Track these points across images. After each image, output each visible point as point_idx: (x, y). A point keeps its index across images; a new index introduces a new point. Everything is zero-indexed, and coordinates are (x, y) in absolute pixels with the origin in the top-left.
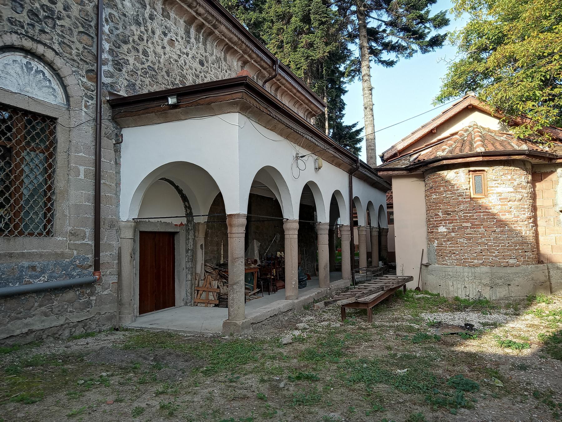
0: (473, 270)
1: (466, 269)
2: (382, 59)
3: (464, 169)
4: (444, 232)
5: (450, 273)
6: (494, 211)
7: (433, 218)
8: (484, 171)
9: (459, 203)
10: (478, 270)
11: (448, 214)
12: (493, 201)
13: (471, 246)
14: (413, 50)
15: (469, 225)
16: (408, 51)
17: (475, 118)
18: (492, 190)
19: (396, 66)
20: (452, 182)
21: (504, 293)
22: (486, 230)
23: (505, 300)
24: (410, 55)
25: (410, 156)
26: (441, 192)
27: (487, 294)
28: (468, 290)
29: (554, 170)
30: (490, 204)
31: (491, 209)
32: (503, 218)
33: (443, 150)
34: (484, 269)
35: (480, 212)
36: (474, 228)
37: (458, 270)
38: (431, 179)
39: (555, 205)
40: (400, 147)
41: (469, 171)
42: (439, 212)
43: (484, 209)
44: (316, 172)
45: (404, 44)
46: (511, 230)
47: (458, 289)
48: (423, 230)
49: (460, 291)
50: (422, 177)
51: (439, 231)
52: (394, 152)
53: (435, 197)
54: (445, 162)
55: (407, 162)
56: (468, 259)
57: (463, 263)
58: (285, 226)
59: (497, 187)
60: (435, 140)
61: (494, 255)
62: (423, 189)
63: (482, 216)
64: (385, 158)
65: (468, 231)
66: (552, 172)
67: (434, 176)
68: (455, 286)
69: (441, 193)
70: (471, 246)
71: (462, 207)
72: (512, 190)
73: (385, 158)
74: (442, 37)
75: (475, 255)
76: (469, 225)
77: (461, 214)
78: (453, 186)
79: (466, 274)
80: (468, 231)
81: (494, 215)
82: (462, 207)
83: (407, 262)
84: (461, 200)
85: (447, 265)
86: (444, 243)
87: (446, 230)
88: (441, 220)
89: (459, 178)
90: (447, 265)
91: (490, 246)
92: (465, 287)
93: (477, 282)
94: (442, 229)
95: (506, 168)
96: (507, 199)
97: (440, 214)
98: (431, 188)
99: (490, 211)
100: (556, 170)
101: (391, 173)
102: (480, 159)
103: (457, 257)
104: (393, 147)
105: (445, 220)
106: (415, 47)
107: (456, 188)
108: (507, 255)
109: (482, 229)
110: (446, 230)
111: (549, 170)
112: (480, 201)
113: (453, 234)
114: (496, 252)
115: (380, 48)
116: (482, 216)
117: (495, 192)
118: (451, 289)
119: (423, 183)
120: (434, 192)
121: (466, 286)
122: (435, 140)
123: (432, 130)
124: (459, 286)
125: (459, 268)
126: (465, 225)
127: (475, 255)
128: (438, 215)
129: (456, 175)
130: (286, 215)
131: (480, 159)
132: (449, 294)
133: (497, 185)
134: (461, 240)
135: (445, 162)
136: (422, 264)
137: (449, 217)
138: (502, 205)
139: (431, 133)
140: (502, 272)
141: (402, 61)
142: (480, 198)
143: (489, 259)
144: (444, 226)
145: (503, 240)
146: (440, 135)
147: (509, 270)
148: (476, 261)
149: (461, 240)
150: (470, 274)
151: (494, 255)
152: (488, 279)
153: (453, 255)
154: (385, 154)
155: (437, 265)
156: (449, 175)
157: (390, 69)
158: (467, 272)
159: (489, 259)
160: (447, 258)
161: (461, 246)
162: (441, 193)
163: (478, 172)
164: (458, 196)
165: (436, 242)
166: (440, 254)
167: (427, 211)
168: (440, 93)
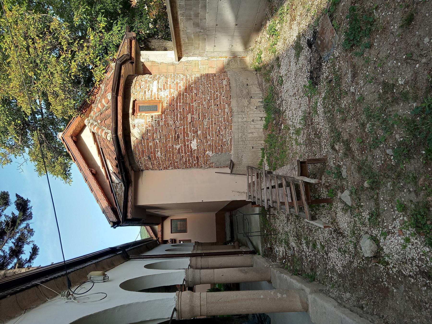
0: (235, 114)
1: (235, 119)
2: (28, 259)
3: (130, 119)
4: (197, 142)
5: (240, 136)
6: (175, 94)
7: (183, 157)
8: (134, 102)
9: (167, 124)
10: (234, 109)
11: (178, 137)
12: (166, 95)
13: (212, 115)
14: (26, 228)
15: (189, 116)
16: (26, 232)
17: (87, 137)
18: (155, 95)
19: (38, 246)
20: (144, 131)
21: (255, 88)
22: (195, 101)
23: (262, 86)
24: (31, 232)
25: (112, 182)
26: (154, 144)
27: (257, 101)
28: (256, 118)
29: (142, 64)
30: (169, 97)
31: (174, 97)
32: (183, 88)
33: (106, 133)
34: (234, 103)
35: (177, 106)
36: (193, 111)
37: (236, 127)
38: (141, 159)
39: (173, 64)
40: (105, 203)
41: (133, 114)
42: (176, 149)
43: (173, 105)
44: (108, 281)
45: (18, 235)
46: (195, 83)
47: (255, 128)
48: (195, 172)
49: (257, 126)
50: (138, 172)
51: (196, 148)
52: (110, 210)
53: (159, 153)
54: (120, 132)
55: (119, 186)
56: (224, 117)
57: (229, 123)
58: (186, 316)
59: (152, 91)
60: (103, 171)
61: (219, 95)
62: (150, 172)
63: (181, 104)
64: (115, 220)
65: (196, 116)
66: (144, 65)
67: (136, 154)
68: (253, 131)
69: (155, 146)
70: (212, 115)
71: (171, 123)
72: (156, 82)
73: (115, 220)
74: (18, 200)
75: (220, 111)
76: (189, 116)
77: (178, 123)
78: (147, 131)
79: (240, 120)
80: (196, 116)
81: (179, 94)
82: (171, 123)
83: (229, 188)
84: (163, 123)
85: (231, 139)
86: (209, 143)
87: (195, 140)
88: (185, 145)
89: (139, 125)
90: (231, 139)
91: (211, 97)
92: (253, 121)
93: (246, 110)
94: (194, 145)
95: (133, 84)
96: (164, 85)
97: (178, 147)
98: (150, 158)
99: (175, 97)
100: (142, 62)
101: (129, 204)
102: (120, 98)
103: (222, 128)
104: (104, 212)
105: (184, 141)
106: (23, 225)
107: (150, 128)
108: (219, 85)
109: (194, 104)
110: (195, 140)
111: (142, 67)
112: (165, 105)
113: (199, 132)
114: (216, 93)
115: (15, 260)
116: (181, 104)
117: (156, 93)
118: (255, 135)
119: (145, 173)
120: (155, 154)
121: (252, 119)
122: (103, 171)
123: (93, 174)
124: (252, 126)
125: (234, 126)
126: (189, 120)
127: (220, 111)
128: (179, 149)
129: (136, 128)
130: (167, 315)
131: (120, 98)
132: (261, 137)
133: (150, 91)
134: (205, 124)
135: (120, 132)
136: (231, 173)
137: (181, 136)
138: (170, 88)
139: (96, 175)
140: (235, 90)
141: (35, 239)
142: (162, 106)
143: (223, 100)
144: (191, 143)
145: (204, 88)
146: (99, 167)
147: (233, 84)
148: (226, 110)
149: (205, 124)
150: (240, 116)
151: (219, 95)
152: (243, 100)
153: (221, 133)
154: (111, 220)
155: (232, 152)
156: (135, 134)
157: (40, 252)
158: (237, 119)
159: (223, 100)
160: (224, 140)
161: (212, 124)
162: (155, 146)
163: (135, 108)
164: (159, 125)
165: (207, 152)
166: (220, 147)
167: (175, 168)
168: (59, 177)
